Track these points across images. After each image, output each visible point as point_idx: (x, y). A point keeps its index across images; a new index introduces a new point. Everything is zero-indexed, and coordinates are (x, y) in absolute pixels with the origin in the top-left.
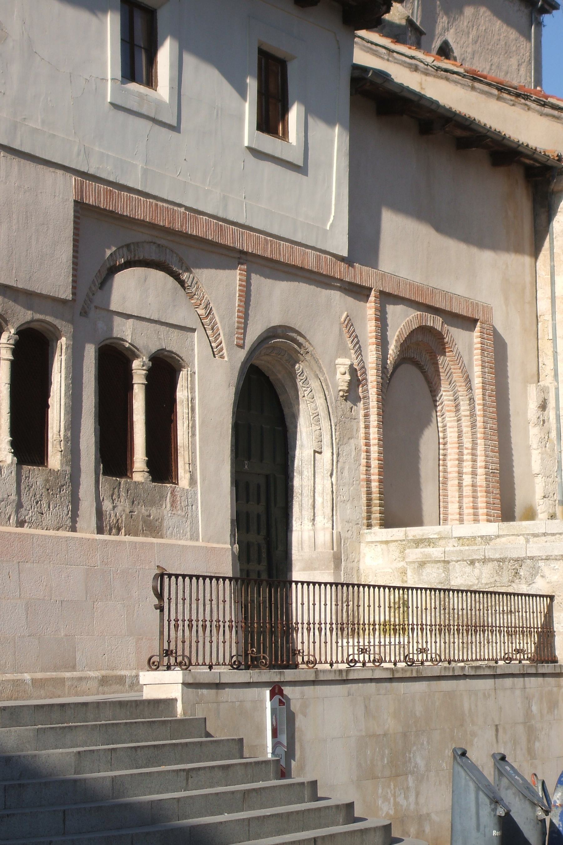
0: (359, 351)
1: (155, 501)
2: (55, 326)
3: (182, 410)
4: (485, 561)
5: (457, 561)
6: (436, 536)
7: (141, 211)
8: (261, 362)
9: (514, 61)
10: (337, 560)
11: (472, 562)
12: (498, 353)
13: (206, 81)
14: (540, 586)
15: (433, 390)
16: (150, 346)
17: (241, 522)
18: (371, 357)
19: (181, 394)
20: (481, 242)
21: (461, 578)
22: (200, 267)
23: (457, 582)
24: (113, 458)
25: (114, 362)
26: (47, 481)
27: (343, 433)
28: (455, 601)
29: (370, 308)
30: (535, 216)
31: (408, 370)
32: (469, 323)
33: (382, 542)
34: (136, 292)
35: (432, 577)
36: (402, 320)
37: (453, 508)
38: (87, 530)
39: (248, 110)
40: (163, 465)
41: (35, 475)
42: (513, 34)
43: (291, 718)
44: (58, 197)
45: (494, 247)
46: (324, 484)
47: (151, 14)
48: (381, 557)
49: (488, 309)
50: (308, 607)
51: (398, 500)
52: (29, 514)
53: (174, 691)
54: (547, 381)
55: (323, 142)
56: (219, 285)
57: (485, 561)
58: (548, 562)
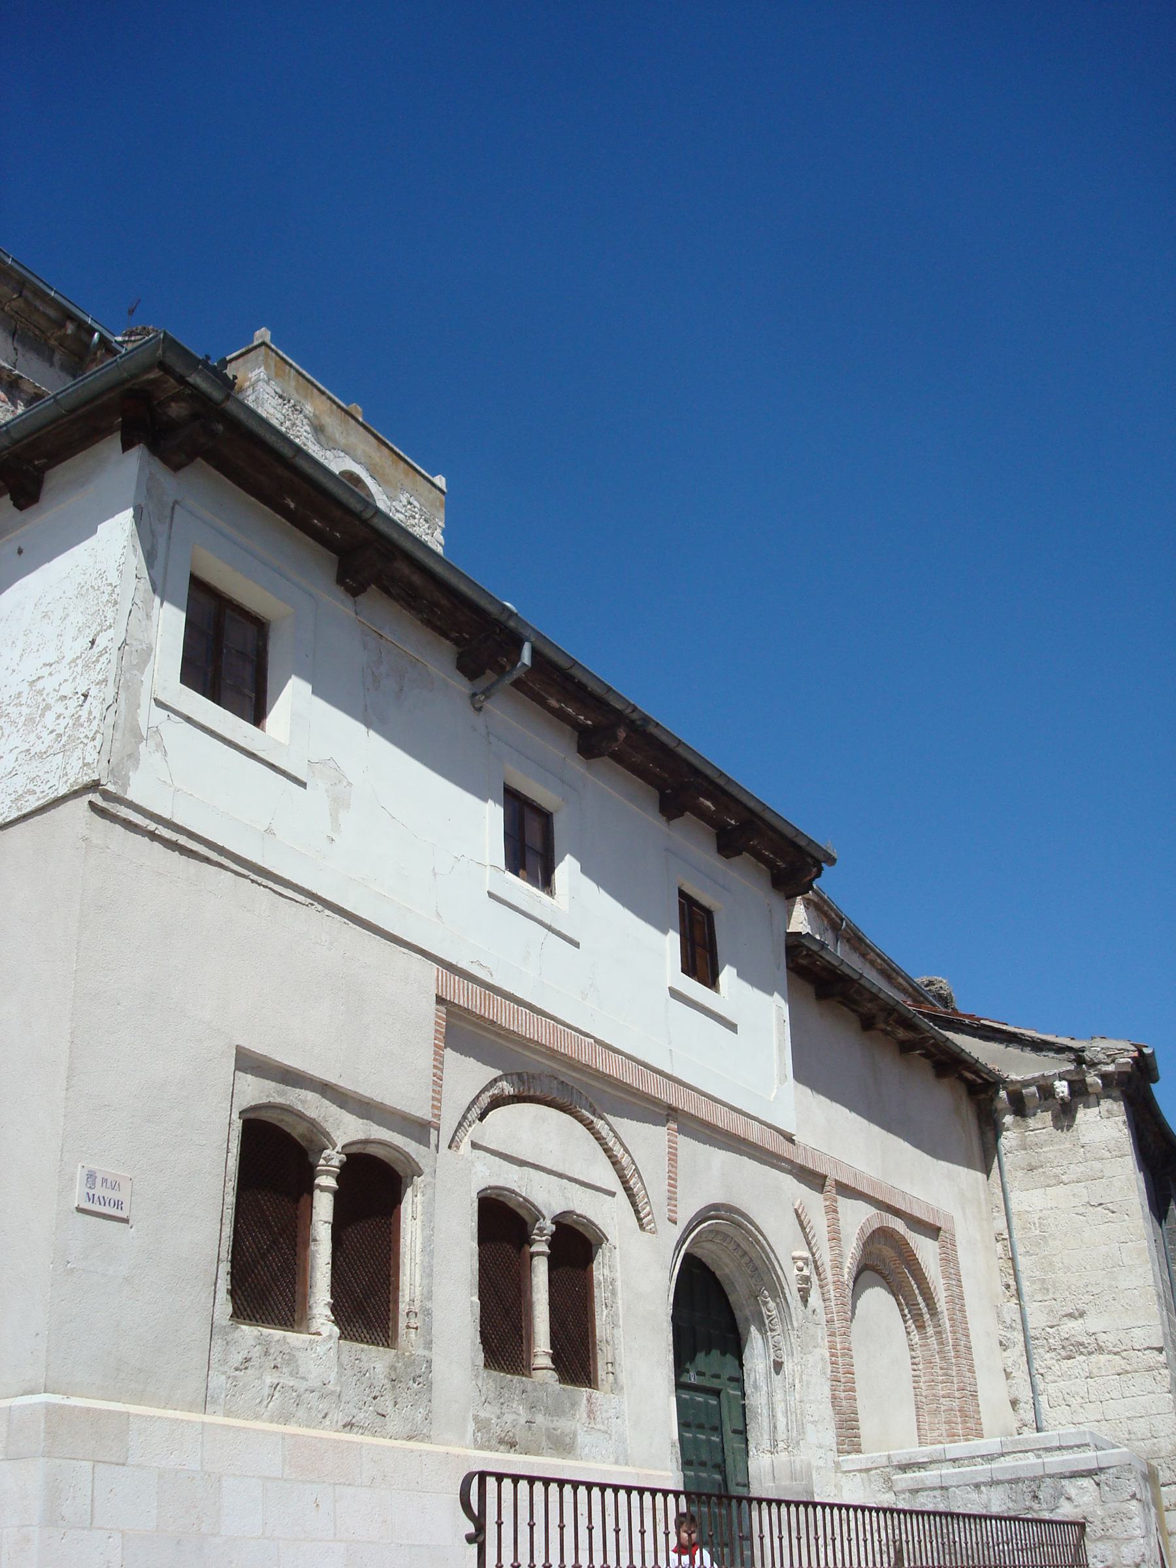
2: (407, 1156)
4: (993, 1483)
5: (958, 1487)
6: (926, 1460)
8: (706, 1253)
11: (977, 1486)
14: (1066, 1511)
16: (553, 1204)
24: (502, 1343)
26: (393, 1368)
28: (961, 1533)
30: (982, 1134)
33: (860, 1471)
40: (577, 1359)
57: (993, 1483)
58: (1073, 1480)
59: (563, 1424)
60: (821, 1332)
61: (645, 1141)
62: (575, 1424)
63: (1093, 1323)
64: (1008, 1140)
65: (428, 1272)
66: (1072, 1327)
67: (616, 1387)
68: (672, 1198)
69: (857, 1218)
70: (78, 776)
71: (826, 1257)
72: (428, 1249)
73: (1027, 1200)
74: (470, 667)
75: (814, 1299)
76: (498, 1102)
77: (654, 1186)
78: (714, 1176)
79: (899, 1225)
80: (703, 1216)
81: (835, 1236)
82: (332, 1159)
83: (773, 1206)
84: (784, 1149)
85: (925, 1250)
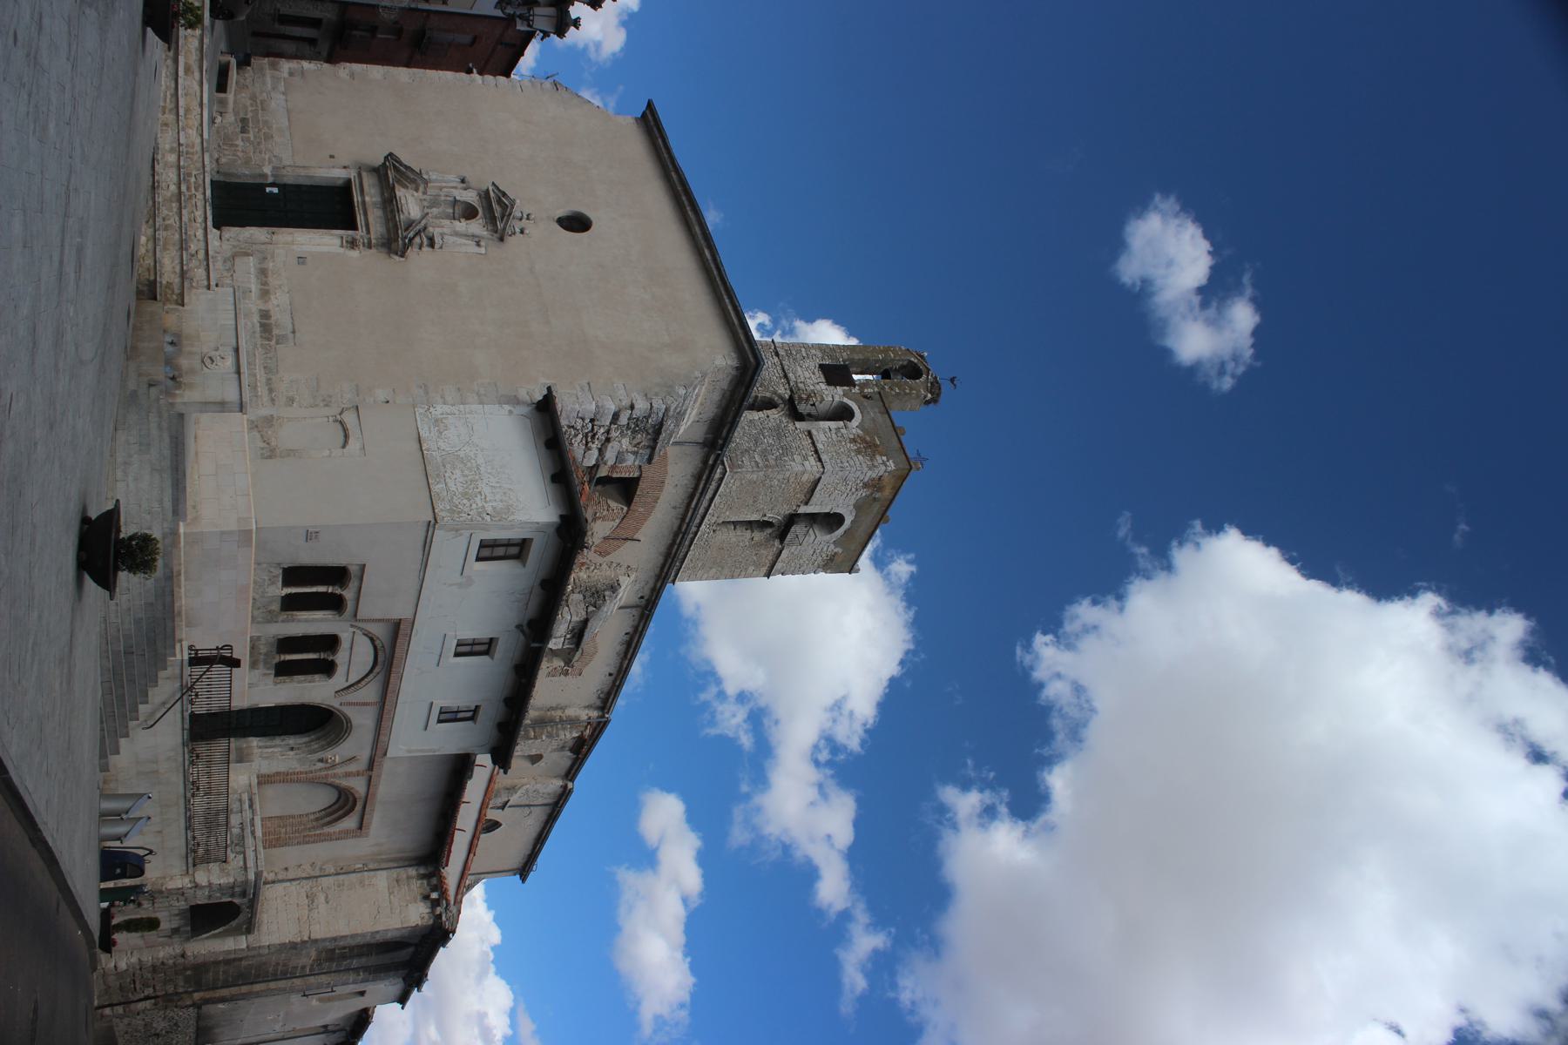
14: (231, 856)
17: (255, 712)
21: (235, 820)
35: (235, 806)
40: (284, 670)
44: (400, 611)
59: (261, 665)
60: (306, 768)
61: (370, 692)
62: (261, 670)
63: (323, 907)
64: (412, 872)
65: (306, 621)
66: (322, 898)
67: (276, 683)
68: (350, 704)
69: (358, 786)
70: (440, 514)
71: (340, 770)
72: (314, 620)
73: (382, 880)
74: (531, 623)
75: (320, 765)
76: (372, 640)
77: (352, 697)
78: (362, 721)
79: (359, 807)
80: (349, 721)
81: (348, 775)
82: (338, 591)
83: (356, 746)
84: (379, 753)
85: (350, 822)
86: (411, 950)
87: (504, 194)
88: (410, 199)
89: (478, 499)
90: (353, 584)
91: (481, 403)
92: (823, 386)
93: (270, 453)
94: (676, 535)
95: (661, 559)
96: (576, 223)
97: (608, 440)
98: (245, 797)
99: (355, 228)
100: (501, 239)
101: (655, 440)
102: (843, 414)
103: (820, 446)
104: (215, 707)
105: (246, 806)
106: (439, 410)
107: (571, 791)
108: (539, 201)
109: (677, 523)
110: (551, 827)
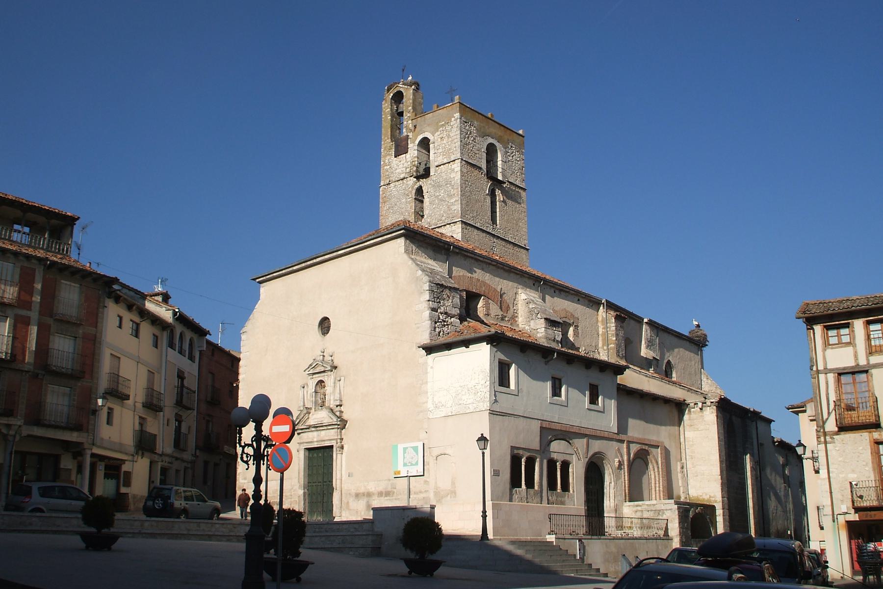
0: (622, 457)
1: (564, 496)
3: (570, 474)
7: (558, 427)
9: (693, 363)
10: (616, 511)
12: (667, 454)
13: (575, 393)
14: (665, 517)
15: (647, 464)
17: (588, 501)
18: (625, 458)
19: (570, 470)
20: (661, 424)
21: (646, 515)
22: (365, 522)
23: (645, 516)
24: (552, 486)
25: (552, 464)
27: (618, 477)
28: (644, 521)
29: (625, 445)
31: (638, 460)
32: (657, 447)
34: (558, 448)
35: (639, 515)
36: (634, 448)
37: (654, 496)
38: (545, 504)
39: (587, 399)
40: (565, 487)
41: (531, 491)
42: (692, 355)
43: (584, 547)
44: (536, 426)
45: (665, 425)
46: (612, 491)
47: (560, 380)
48: (629, 510)
49: (663, 443)
50: (609, 522)
51: (635, 493)
52: (529, 500)
53: (554, 540)
54: (684, 461)
55: (609, 406)
56: (580, 444)
78: (597, 446)
86: (734, 418)
87: (311, 365)
88: (314, 416)
89: (478, 387)
90: (521, 452)
91: (427, 383)
92: (408, 155)
93: (453, 493)
94: (498, 268)
95: (512, 275)
96: (325, 325)
97: (446, 313)
98: (636, 508)
99: (332, 447)
100: (336, 368)
101: (446, 287)
102: (425, 144)
103: (446, 161)
104: (583, 521)
105: (639, 508)
106: (430, 405)
107: (650, 320)
108: (313, 345)
109: (491, 267)
110: (672, 330)
